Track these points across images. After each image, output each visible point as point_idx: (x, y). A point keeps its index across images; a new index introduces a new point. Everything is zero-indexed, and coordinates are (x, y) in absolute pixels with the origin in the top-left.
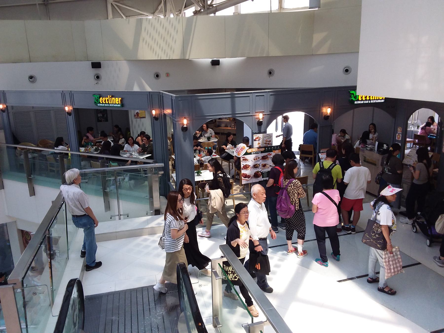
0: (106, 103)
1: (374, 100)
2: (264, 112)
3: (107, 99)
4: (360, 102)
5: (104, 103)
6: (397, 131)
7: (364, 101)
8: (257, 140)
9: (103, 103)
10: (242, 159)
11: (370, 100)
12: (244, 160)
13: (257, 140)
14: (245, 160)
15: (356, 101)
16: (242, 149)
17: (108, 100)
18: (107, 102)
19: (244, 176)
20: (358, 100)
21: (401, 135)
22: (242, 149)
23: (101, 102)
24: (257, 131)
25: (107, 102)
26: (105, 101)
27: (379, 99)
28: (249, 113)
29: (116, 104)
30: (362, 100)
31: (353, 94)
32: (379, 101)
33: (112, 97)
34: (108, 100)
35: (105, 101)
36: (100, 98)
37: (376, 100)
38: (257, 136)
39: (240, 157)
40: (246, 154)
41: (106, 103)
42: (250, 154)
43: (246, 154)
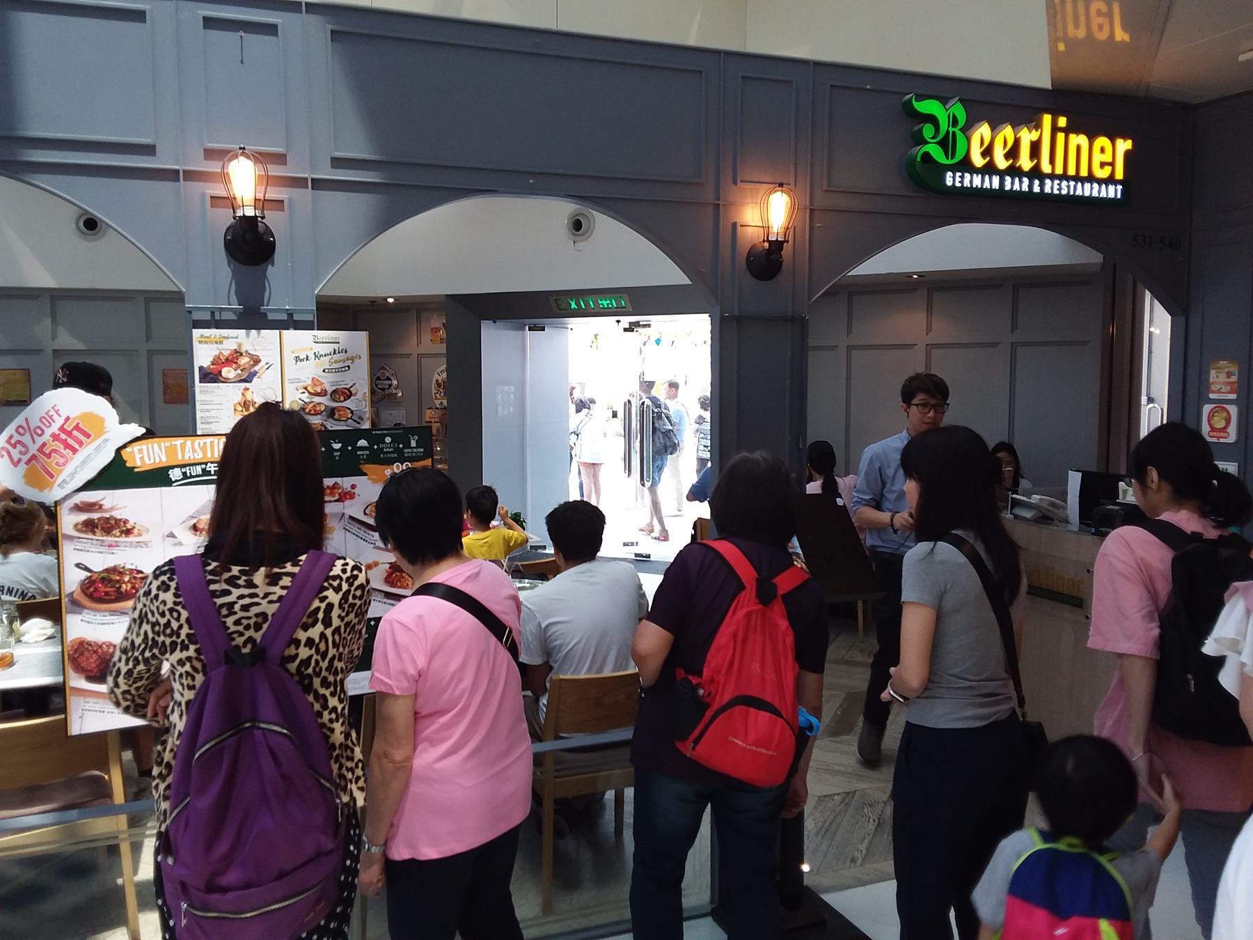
0: (1015, 171)
1: (1065, 177)
2: (280, 159)
3: (1027, 136)
4: (977, 180)
5: (1002, 163)
6: (1203, 389)
7: (1002, 174)
8: (228, 372)
9: (990, 169)
10: (68, 521)
11: (1036, 173)
12: (90, 526)
13: (228, 372)
14: (107, 527)
15: (954, 168)
16: (76, 435)
17: (1035, 148)
18: (1025, 163)
19: (92, 662)
20: (966, 165)
21: (1233, 410)
22: (76, 435)
23: (978, 161)
24: (231, 304)
25: (1025, 163)
26: (1013, 153)
27: (1091, 178)
28: (149, 150)
29: (1091, 178)
30: (990, 169)
31: (932, 119)
32: (1086, 190)
33: (1067, 131)
34: (1035, 148)
35: (1013, 153)
36: (967, 130)
37: (1077, 178)
38: (228, 347)
39: (50, 496)
40: (117, 474)
41: (1015, 171)
42: (158, 477)
43: (117, 474)
